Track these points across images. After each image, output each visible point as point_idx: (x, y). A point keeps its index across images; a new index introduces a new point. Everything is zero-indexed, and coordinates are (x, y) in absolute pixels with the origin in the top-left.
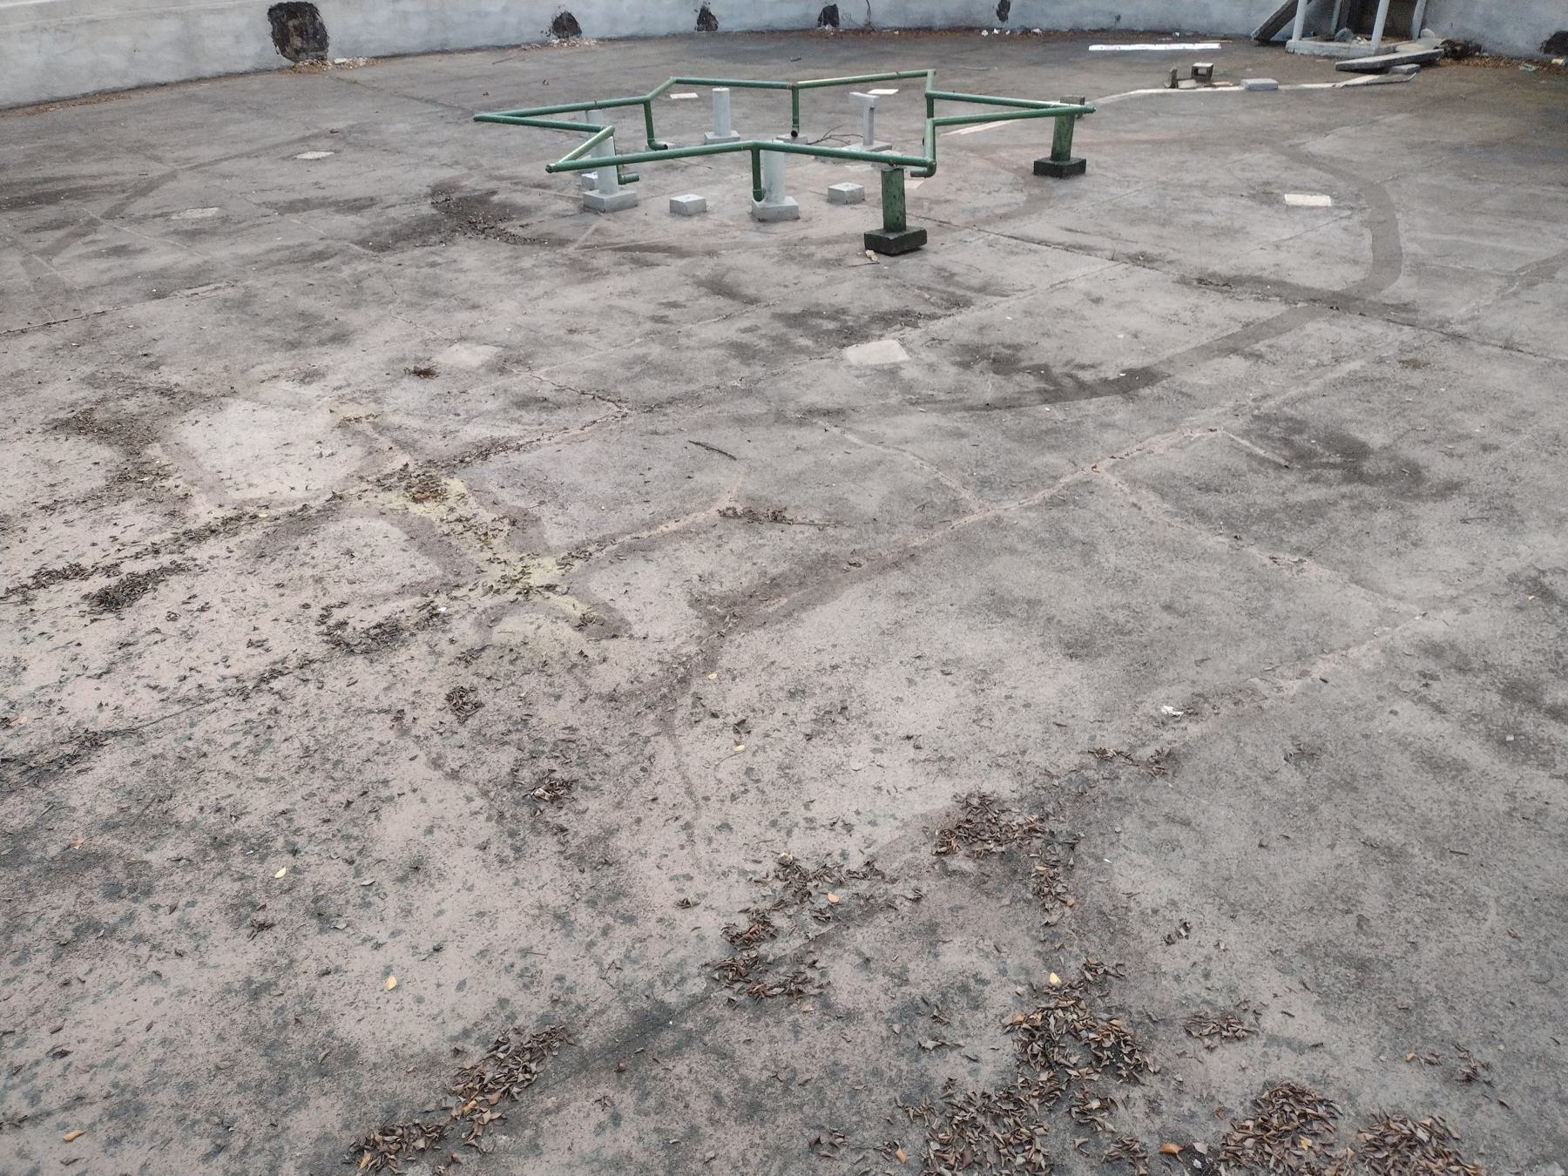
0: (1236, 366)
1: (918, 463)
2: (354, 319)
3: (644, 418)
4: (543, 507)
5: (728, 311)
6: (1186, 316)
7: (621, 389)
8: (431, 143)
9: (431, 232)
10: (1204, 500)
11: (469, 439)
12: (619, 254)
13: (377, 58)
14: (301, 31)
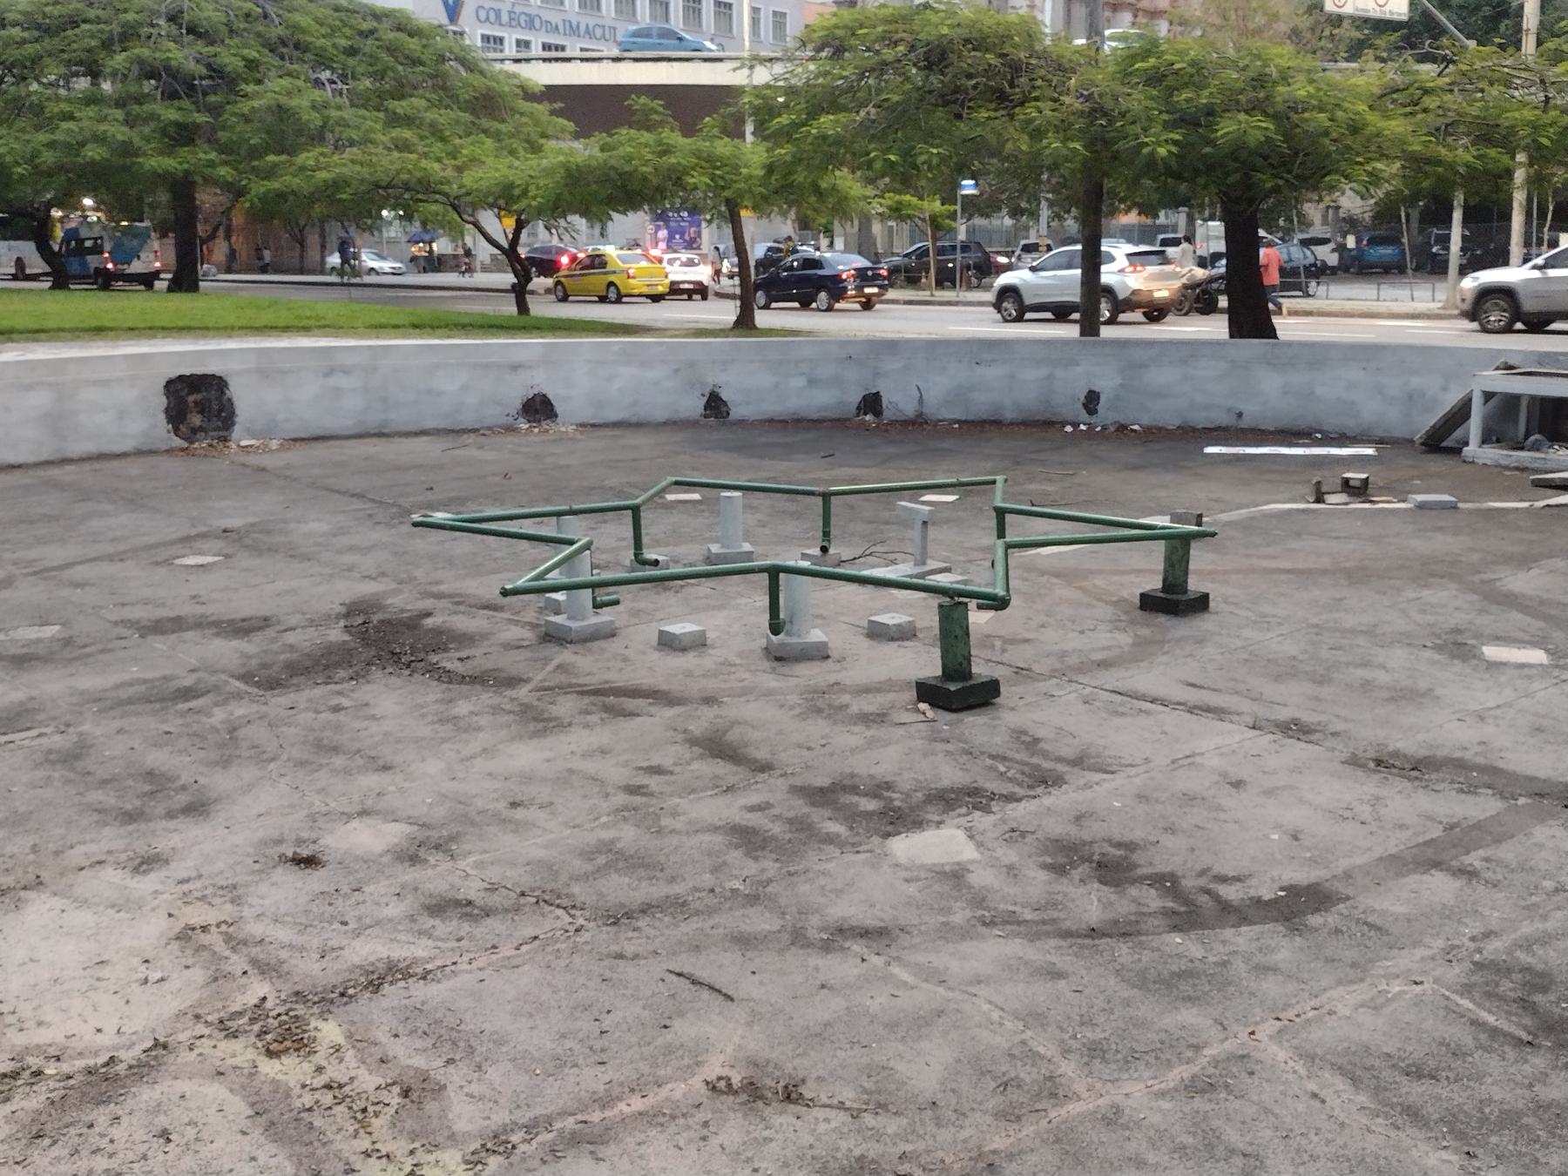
0: (1440, 887)
1: (995, 1015)
2: (220, 782)
3: (606, 933)
4: (451, 1069)
5: (732, 780)
6: (1365, 811)
7: (576, 889)
8: (352, 549)
9: (338, 665)
10: (1416, 1091)
11: (356, 960)
12: (587, 700)
13: (295, 440)
14: (202, 408)
